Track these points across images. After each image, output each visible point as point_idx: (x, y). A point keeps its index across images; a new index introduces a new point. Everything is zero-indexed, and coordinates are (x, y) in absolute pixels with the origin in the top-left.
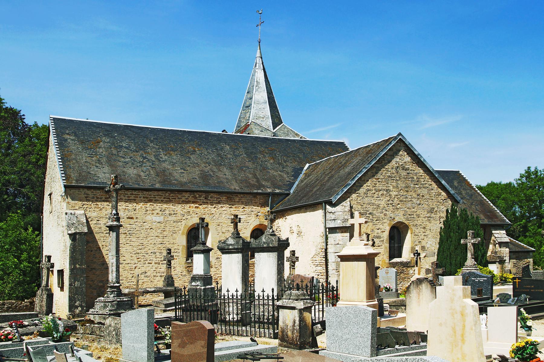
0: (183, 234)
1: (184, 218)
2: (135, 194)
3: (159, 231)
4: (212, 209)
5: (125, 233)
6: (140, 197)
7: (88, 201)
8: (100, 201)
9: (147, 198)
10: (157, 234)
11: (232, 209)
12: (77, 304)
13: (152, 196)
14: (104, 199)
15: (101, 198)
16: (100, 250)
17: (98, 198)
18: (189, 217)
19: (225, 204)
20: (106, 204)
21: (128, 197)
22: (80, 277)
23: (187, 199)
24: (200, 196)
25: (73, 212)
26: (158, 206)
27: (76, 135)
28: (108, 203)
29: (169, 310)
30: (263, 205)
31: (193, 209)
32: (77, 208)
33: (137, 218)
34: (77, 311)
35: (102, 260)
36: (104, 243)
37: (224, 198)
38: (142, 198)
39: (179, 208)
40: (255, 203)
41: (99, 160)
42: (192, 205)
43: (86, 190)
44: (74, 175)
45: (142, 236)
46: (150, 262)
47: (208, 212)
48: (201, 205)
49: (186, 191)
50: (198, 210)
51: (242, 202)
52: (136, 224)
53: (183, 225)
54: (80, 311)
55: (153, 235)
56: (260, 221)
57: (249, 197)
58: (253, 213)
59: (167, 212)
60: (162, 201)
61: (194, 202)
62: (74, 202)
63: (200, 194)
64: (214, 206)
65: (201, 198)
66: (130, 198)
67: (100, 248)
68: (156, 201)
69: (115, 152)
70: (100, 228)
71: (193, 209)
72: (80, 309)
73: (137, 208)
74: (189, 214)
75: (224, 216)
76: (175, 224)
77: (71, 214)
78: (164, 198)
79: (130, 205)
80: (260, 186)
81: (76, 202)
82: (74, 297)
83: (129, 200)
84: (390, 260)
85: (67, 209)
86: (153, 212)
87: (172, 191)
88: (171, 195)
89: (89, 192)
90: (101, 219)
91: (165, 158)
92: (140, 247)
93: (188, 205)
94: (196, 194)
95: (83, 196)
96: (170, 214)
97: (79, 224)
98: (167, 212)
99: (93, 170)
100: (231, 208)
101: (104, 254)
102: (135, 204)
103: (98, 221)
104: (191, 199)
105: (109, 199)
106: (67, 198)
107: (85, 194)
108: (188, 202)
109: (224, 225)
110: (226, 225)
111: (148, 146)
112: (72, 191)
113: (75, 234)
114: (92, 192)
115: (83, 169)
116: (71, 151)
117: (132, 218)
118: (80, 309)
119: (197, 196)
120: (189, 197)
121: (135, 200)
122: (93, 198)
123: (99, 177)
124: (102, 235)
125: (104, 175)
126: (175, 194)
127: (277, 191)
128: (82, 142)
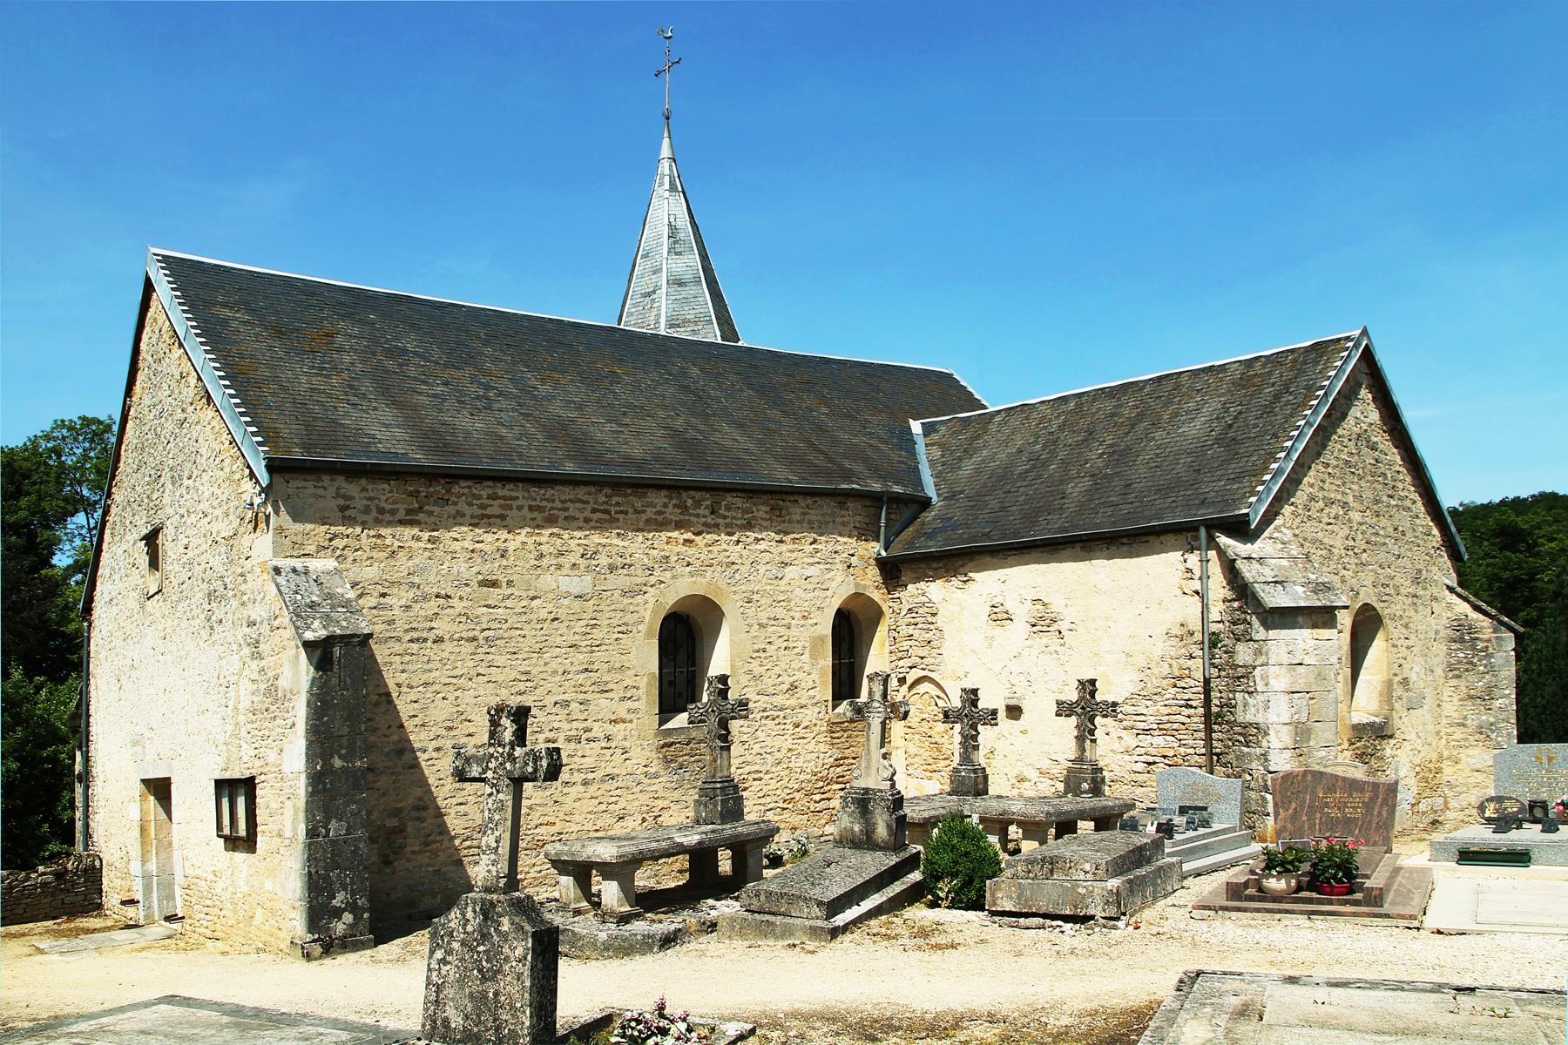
0: (649, 635)
1: (653, 580)
2: (505, 498)
3: (579, 627)
4: (731, 548)
5: (474, 639)
6: (520, 508)
7: (349, 521)
8: (389, 524)
9: (540, 509)
10: (572, 639)
11: (784, 547)
12: (338, 900)
13: (558, 504)
14: (401, 514)
15: (393, 512)
16: (390, 701)
17: (381, 511)
18: (668, 574)
19: (766, 529)
20: (409, 532)
21: (483, 507)
22: (347, 804)
23: (660, 513)
24: (698, 504)
25: (298, 564)
26: (575, 540)
27: (249, 310)
28: (415, 531)
29: (845, 929)
30: (866, 532)
31: (677, 549)
32: (311, 549)
33: (510, 583)
34: (340, 927)
35: (395, 738)
36: (402, 678)
37: (762, 511)
38: (525, 511)
39: (636, 546)
40: (844, 524)
41: (351, 387)
42: (675, 534)
43: (341, 481)
44: (289, 430)
45: (525, 645)
46: (551, 735)
47: (721, 558)
48: (698, 534)
49: (658, 486)
50: (691, 551)
51: (810, 522)
52: (509, 603)
53: (650, 606)
54: (351, 926)
55: (559, 640)
56: (857, 585)
57: (828, 505)
58: (838, 558)
59: (603, 560)
60: (587, 520)
61: (679, 526)
62: (299, 527)
63: (698, 495)
64: (735, 538)
65: (701, 511)
66: (489, 511)
67: (388, 694)
68: (569, 522)
69: (390, 364)
70: (391, 622)
71: (677, 549)
72: (348, 917)
73: (512, 546)
74: (673, 563)
75: (762, 569)
76: (626, 601)
77: (294, 570)
78: (594, 511)
79: (489, 538)
80: (848, 476)
81: (309, 526)
82: (326, 878)
83: (483, 516)
84: (661, 724)
85: (276, 554)
86: (561, 560)
87: (617, 485)
88: (615, 499)
89: (352, 489)
90: (395, 590)
91: (544, 389)
92: (522, 686)
93: (664, 535)
94: (684, 495)
95: (333, 504)
96: (612, 568)
97: (333, 607)
98: (603, 560)
99: (349, 417)
100: (781, 541)
101: (404, 717)
102: (503, 534)
103: (383, 595)
104: (671, 513)
105: (421, 517)
106: (277, 512)
107: (338, 495)
108: (661, 525)
109: (763, 601)
110: (769, 601)
111: (481, 353)
112: (294, 484)
113: (330, 640)
114: (364, 490)
115: (311, 411)
116: (252, 356)
117: (494, 584)
118: (348, 917)
119: (690, 502)
120: (665, 505)
121: (503, 517)
122: (367, 510)
123: (374, 437)
124: (398, 647)
125: (385, 433)
126: (626, 495)
127: (897, 489)
128: (279, 333)
